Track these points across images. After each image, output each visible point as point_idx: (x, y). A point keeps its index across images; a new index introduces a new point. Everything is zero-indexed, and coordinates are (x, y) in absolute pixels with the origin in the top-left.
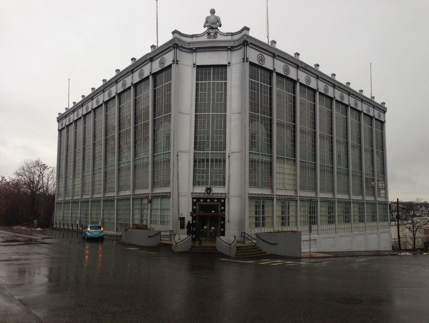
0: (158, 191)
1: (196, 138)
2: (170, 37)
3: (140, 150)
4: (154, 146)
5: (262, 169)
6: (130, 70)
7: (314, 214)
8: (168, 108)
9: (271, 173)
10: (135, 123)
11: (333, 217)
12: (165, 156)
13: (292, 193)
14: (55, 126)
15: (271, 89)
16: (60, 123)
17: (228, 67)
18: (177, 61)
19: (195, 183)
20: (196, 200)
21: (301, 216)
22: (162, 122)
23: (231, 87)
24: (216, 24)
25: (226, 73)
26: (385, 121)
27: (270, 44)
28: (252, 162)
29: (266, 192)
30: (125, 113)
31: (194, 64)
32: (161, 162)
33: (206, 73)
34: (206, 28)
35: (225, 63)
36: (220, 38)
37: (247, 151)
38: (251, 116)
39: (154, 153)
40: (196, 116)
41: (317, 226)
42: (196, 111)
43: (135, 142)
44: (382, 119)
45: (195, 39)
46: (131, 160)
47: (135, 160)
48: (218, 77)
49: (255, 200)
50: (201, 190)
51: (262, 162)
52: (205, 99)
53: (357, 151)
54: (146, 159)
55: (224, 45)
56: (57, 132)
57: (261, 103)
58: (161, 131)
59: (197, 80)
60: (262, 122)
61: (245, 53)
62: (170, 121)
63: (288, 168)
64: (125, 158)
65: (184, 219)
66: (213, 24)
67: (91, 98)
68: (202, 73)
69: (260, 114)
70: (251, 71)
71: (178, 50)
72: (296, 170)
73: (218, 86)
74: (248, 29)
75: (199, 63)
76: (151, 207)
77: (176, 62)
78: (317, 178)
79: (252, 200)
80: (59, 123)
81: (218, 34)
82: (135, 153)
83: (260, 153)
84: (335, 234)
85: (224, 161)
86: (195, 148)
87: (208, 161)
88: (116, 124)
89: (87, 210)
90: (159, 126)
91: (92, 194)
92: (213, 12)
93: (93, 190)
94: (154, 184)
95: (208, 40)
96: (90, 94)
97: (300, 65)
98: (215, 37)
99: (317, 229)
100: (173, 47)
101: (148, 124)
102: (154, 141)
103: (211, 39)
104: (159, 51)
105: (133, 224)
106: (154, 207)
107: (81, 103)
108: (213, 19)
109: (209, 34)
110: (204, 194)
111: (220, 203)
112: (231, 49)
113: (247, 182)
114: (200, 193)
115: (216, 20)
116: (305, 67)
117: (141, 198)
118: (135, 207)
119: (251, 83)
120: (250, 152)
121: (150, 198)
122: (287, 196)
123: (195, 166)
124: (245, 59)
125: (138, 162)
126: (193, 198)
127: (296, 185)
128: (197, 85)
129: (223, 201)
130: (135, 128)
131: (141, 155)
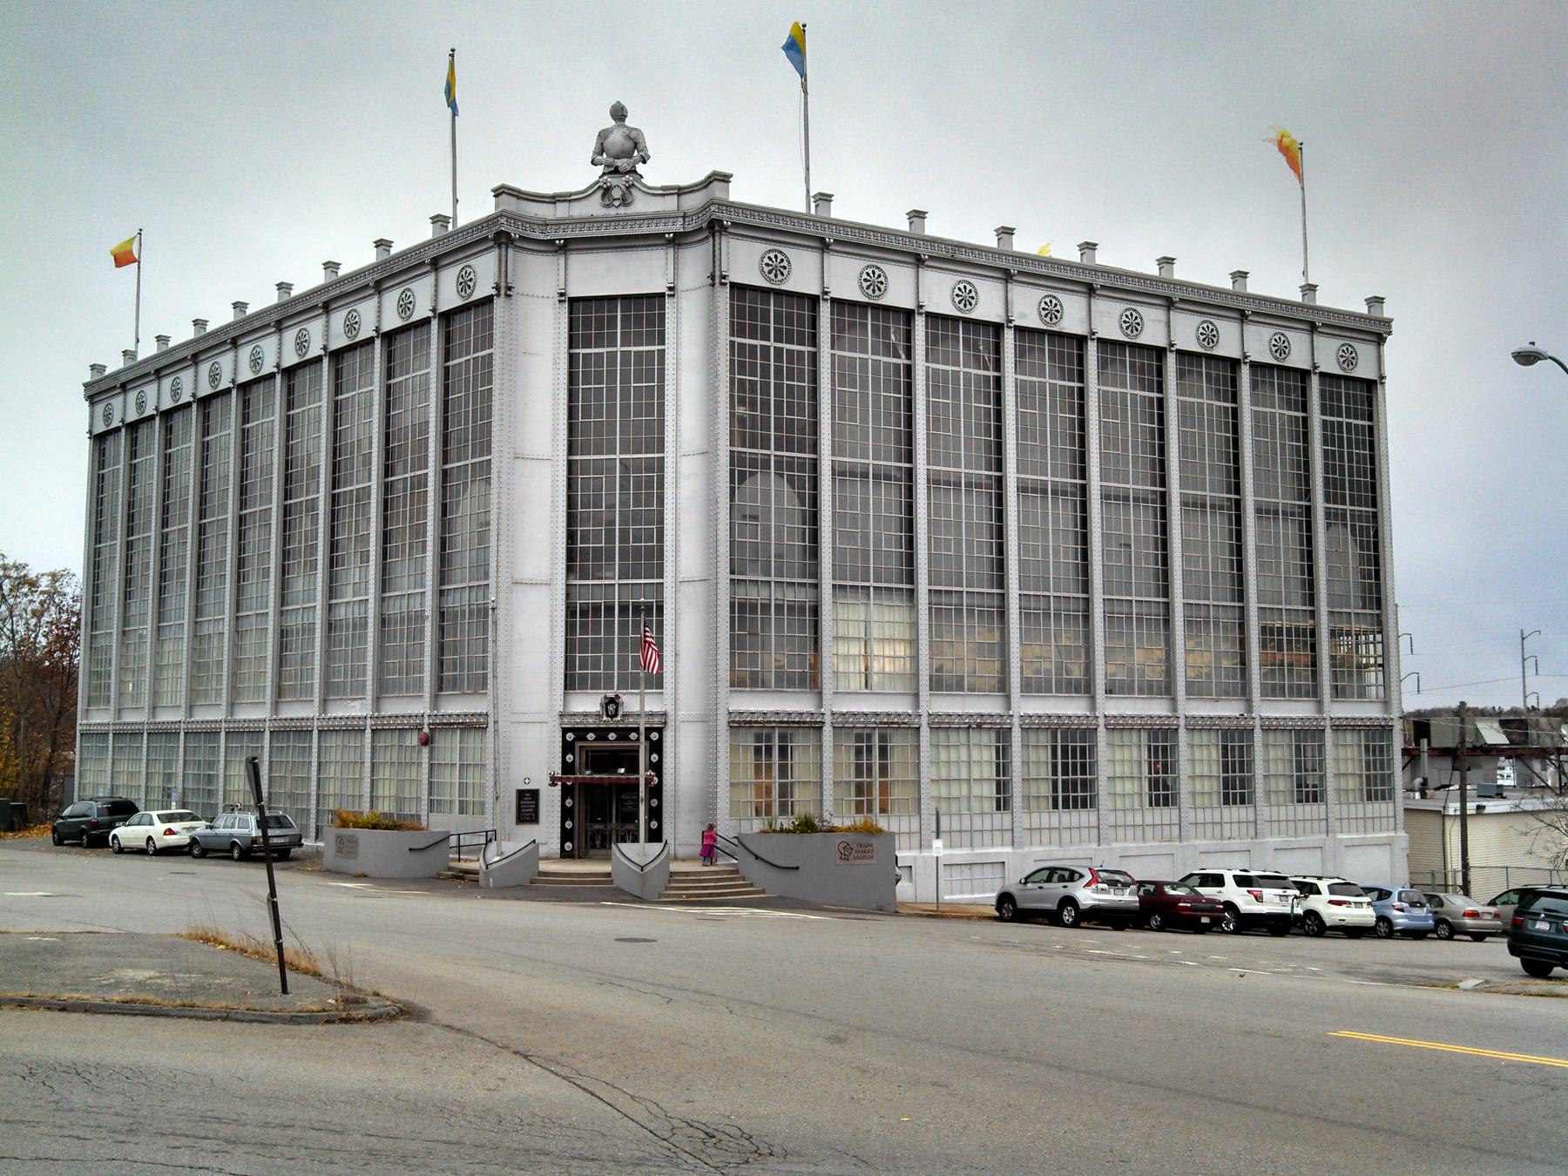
0: (455, 707)
1: (571, 536)
4: (444, 560)
5: (779, 627)
6: (370, 279)
7: (1242, 770)
9: (816, 642)
10: (388, 470)
11: (1247, 782)
13: (901, 706)
14: (76, 420)
16: (100, 408)
17: (668, 302)
19: (571, 683)
20: (574, 737)
21: (1193, 778)
24: (630, 156)
26: (1382, 377)
28: (742, 611)
29: (796, 704)
30: (353, 430)
31: (562, 295)
32: (463, 612)
33: (600, 321)
34: (600, 169)
35: (660, 288)
36: (642, 205)
40: (570, 464)
42: (570, 451)
43: (386, 537)
44: (1364, 371)
45: (561, 211)
46: (371, 596)
49: (753, 731)
50: (588, 704)
51: (779, 608)
53: (1216, 527)
54: (418, 599)
55: (653, 229)
56: (84, 446)
57: (864, 397)
58: (465, 510)
59: (572, 343)
60: (779, 475)
61: (715, 258)
62: (488, 481)
63: (887, 618)
64: (350, 588)
66: (621, 156)
67: (231, 338)
68: (587, 322)
69: (772, 452)
70: (737, 312)
71: (510, 251)
72: (914, 625)
73: (638, 362)
74: (725, 178)
76: (431, 758)
77: (505, 289)
79: (742, 731)
80: (92, 404)
81: (633, 191)
82: (384, 573)
83: (773, 578)
84: (1094, 845)
85: (660, 609)
86: (570, 570)
87: (610, 609)
88: (323, 461)
89: (212, 764)
91: (154, 709)
92: (619, 113)
94: (440, 684)
96: (228, 326)
98: (625, 202)
101: (422, 481)
102: (443, 544)
103: (612, 212)
104: (455, 245)
107: (275, 317)
108: (617, 139)
109: (607, 191)
110: (598, 715)
112: (677, 241)
113: (724, 674)
114: (585, 715)
115: (628, 145)
117: (401, 728)
118: (380, 758)
119: (736, 350)
120: (736, 577)
121: (426, 730)
122: (877, 714)
123: (570, 628)
124: (715, 278)
125: (452, 602)
126: (565, 731)
127: (916, 675)
128: (572, 359)
130: (387, 488)
131: (403, 585)
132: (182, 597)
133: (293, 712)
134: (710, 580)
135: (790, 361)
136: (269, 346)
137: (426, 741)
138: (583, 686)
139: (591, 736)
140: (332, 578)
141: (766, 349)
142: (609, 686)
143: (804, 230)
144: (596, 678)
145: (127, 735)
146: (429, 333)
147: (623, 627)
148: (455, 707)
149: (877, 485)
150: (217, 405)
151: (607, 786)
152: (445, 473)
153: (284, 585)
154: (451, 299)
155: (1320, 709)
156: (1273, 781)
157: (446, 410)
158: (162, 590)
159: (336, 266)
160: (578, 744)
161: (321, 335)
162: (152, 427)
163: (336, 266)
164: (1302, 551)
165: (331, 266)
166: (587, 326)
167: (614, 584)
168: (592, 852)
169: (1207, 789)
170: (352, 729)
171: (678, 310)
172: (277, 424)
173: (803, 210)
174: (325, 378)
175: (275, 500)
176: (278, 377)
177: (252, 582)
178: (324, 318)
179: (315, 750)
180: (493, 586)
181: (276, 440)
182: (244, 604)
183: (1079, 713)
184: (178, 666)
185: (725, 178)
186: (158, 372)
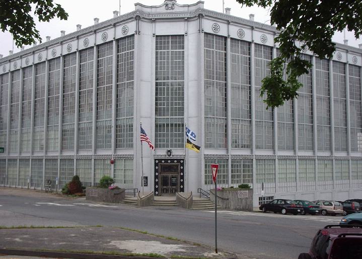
0: (122, 152)
1: (156, 104)
2: (132, 9)
3: (103, 113)
6: (93, 29)
8: (131, 75)
12: (128, 120)
15: (226, 55)
18: (139, 32)
20: (158, 162)
22: (125, 88)
23: (188, 56)
25: (183, 42)
27: (225, 13)
31: (154, 34)
33: (165, 42)
36: (177, 9)
37: (203, 116)
38: (206, 83)
39: (117, 117)
41: (274, 184)
47: (97, 122)
48: (168, 85)
50: (162, 153)
52: (164, 67)
55: (181, 16)
57: (216, 69)
58: (124, 96)
65: (146, 178)
70: (206, 41)
71: (140, 21)
73: (176, 54)
74: (203, 3)
75: (157, 34)
76: (114, 167)
77: (138, 32)
78: (314, 136)
81: (175, 5)
82: (63, 118)
90: (122, 92)
91: (20, 153)
93: (21, 149)
94: (116, 146)
95: (166, 11)
97: (254, 26)
99: (295, 185)
100: (135, 18)
101: (58, 97)
103: (169, 11)
105: (94, 184)
106: (117, 167)
107: (32, 51)
109: (167, 5)
111: (179, 164)
112: (188, 20)
116: (260, 27)
117: (103, 159)
122: (242, 155)
123: (156, 131)
124: (200, 30)
125: (99, 124)
126: (155, 160)
129: (182, 161)
132: (29, 121)
133: (67, 154)
134: (198, 117)
135: (219, 55)
136: (31, 58)
137: (113, 162)
138: (160, 147)
139: (175, 161)
140: (79, 115)
141: (213, 51)
142: (167, 146)
143: (223, 18)
144: (164, 145)
145: (24, 161)
146: (8, 77)
147: (172, 130)
148: (122, 152)
149: (242, 91)
150: (16, 73)
151: (169, 174)
152: (117, 85)
153: (63, 117)
154: (120, 35)
155: (348, 154)
156: (301, 174)
157: (118, 67)
158: (22, 119)
159: (98, 20)
160: (159, 164)
161: (75, 46)
162: (112, 44)
163: (98, 20)
164: (310, 116)
165: (79, 26)
166: (161, 44)
167: (169, 118)
168: (163, 194)
169: (283, 177)
170: (88, 159)
171: (188, 40)
172: (46, 75)
173: (222, 12)
174: (61, 61)
175: (32, 99)
176: (33, 66)
177: (52, 115)
178: (9, 64)
179: (75, 165)
180: (135, 118)
181: (20, 86)
182: (50, 123)
183: (223, 154)
184: (16, 141)
185: (203, 3)
186: (21, 56)
